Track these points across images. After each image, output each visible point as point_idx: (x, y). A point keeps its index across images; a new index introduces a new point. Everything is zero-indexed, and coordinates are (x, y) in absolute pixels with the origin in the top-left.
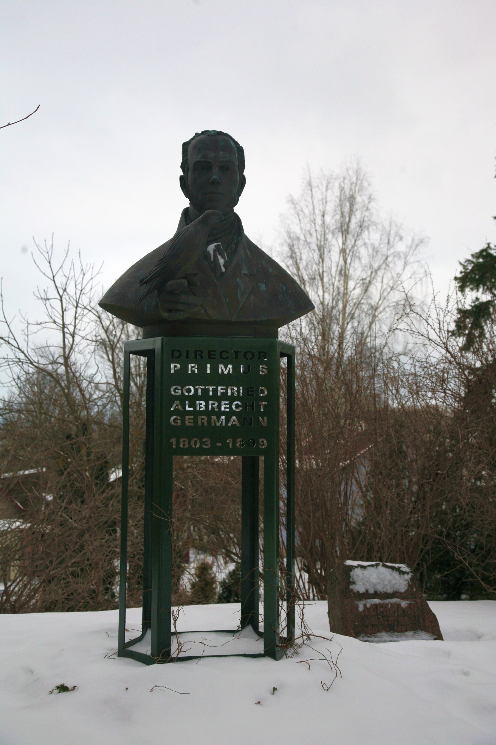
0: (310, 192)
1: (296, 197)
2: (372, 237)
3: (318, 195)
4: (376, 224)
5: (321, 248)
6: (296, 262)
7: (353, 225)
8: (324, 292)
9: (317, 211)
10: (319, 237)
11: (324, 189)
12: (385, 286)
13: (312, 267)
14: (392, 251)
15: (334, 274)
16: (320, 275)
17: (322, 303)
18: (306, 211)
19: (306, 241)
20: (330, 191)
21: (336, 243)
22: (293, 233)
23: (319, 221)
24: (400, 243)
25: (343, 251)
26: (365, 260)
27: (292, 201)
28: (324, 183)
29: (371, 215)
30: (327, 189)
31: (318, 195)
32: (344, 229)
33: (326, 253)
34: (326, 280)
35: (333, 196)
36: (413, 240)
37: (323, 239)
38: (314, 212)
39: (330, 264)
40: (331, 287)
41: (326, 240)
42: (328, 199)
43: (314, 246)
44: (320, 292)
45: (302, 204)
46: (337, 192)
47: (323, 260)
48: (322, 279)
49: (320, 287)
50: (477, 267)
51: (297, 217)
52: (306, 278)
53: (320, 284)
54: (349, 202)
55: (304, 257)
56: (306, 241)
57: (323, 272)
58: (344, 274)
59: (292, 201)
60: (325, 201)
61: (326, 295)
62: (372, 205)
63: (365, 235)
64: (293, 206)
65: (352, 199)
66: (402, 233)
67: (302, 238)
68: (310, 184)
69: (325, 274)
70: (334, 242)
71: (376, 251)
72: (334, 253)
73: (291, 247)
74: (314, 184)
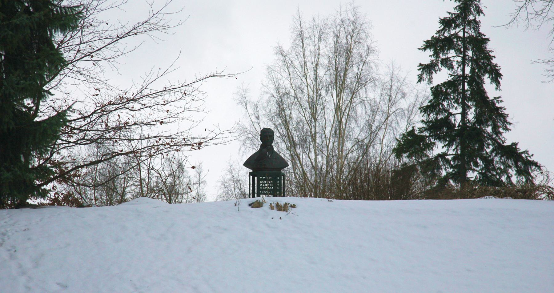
0: (302, 44)
1: (286, 48)
2: (372, 94)
3: (310, 48)
4: (373, 80)
5: (313, 106)
6: (286, 121)
7: (350, 78)
8: (316, 155)
9: (309, 64)
10: (311, 94)
11: (317, 40)
12: (385, 149)
13: (303, 128)
14: (393, 109)
15: (328, 135)
16: (312, 136)
17: (315, 168)
18: (296, 63)
19: (296, 97)
20: (323, 43)
21: (330, 100)
22: (283, 88)
23: (311, 74)
24: (402, 101)
25: (338, 108)
26: (362, 122)
27: (281, 52)
28: (317, 34)
29: (370, 68)
30: (320, 40)
31: (310, 48)
32: (339, 82)
33: (319, 110)
34: (318, 141)
35: (327, 49)
36: (417, 97)
37: (315, 96)
38: (306, 65)
39: (324, 122)
40: (325, 149)
41: (319, 95)
42: (321, 52)
43: (306, 105)
44: (312, 155)
45: (292, 56)
46: (331, 41)
47: (316, 120)
48: (314, 140)
49: (312, 150)
50: (407, 142)
51: (287, 70)
52: (296, 139)
53: (311, 146)
54: (344, 52)
55: (294, 116)
56: (296, 97)
57: (316, 133)
58: (340, 133)
59: (281, 52)
60: (318, 55)
61: (319, 158)
62: (371, 58)
63: (362, 92)
64: (282, 58)
65: (348, 52)
66: (406, 90)
67: (292, 93)
68: (301, 35)
69: (318, 135)
70: (328, 98)
71: (374, 111)
72: (328, 111)
73: (280, 104)
74: (306, 35)
